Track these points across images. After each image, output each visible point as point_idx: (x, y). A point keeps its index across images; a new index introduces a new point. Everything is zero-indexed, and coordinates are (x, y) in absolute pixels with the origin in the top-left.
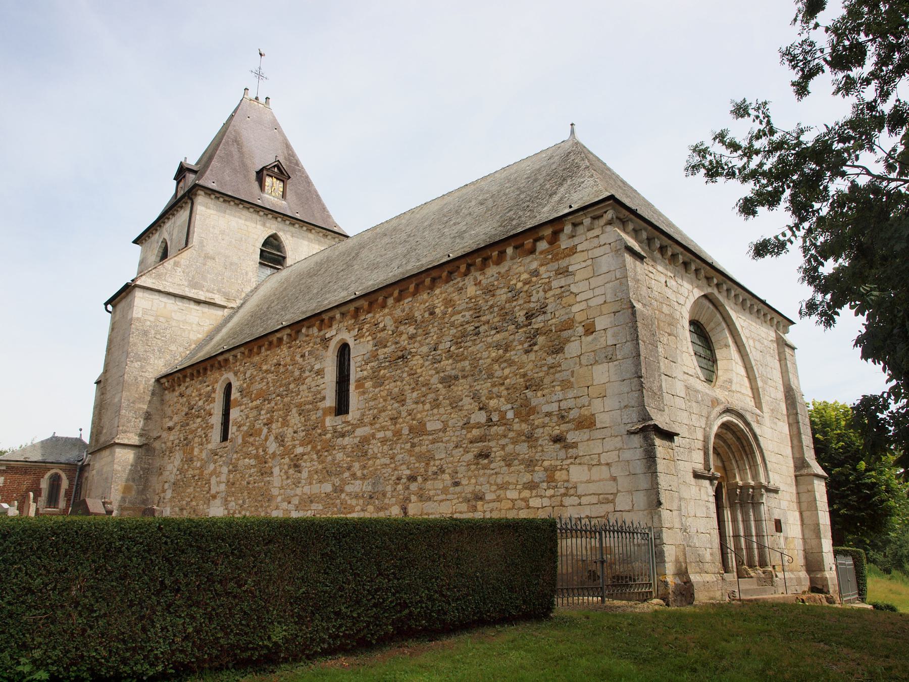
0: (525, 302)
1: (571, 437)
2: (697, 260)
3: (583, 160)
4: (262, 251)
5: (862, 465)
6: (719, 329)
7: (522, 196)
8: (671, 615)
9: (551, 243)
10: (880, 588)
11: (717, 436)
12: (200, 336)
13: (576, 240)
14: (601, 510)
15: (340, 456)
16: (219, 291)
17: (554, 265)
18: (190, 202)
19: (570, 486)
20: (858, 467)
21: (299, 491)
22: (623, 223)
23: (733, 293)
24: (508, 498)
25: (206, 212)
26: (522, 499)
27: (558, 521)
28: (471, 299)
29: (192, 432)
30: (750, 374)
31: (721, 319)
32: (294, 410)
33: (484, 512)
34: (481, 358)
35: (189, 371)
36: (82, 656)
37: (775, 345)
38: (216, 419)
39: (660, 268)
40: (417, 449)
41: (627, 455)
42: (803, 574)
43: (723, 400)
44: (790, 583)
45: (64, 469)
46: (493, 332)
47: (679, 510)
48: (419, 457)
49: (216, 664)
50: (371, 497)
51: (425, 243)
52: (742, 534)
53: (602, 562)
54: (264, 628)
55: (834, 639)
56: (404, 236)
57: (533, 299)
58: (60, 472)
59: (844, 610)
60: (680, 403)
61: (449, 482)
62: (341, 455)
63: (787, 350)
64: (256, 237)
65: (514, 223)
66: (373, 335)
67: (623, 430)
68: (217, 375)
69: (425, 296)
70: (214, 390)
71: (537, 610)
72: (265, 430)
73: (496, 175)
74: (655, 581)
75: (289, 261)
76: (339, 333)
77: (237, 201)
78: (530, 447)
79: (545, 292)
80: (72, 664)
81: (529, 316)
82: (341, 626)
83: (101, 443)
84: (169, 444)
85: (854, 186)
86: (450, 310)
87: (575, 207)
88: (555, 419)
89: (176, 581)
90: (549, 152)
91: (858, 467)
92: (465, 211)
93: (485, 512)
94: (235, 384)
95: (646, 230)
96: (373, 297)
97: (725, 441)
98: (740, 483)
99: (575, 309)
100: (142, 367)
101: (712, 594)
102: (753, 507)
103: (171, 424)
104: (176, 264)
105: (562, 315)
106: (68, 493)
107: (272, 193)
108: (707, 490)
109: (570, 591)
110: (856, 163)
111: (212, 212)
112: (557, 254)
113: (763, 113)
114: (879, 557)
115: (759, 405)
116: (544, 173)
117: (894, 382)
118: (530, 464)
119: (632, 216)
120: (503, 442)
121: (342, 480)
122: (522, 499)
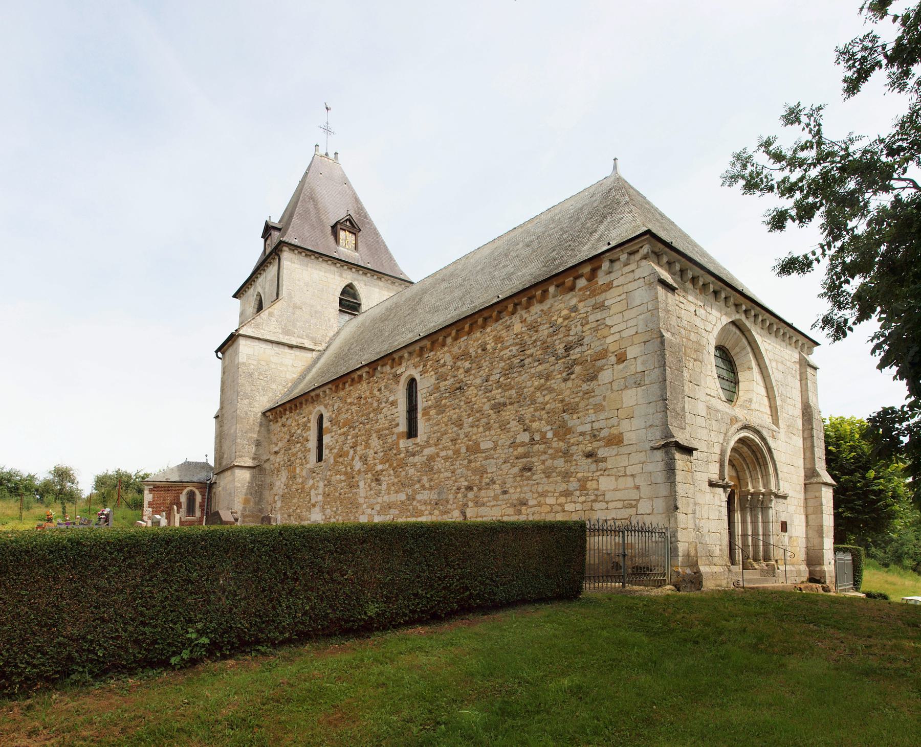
0: (565, 336)
1: (601, 453)
2: (728, 289)
3: (624, 195)
4: (341, 300)
5: (871, 474)
6: (743, 353)
7: (565, 236)
8: (680, 599)
9: (589, 280)
10: (874, 579)
11: (734, 449)
12: (295, 376)
13: (613, 276)
14: (625, 513)
15: (411, 471)
16: (307, 336)
17: (592, 301)
18: (277, 257)
19: (599, 493)
20: (867, 475)
21: (380, 500)
22: (657, 255)
23: (760, 318)
24: (547, 505)
25: (289, 261)
26: (558, 505)
27: (587, 522)
28: (517, 335)
29: (294, 455)
30: (770, 393)
31: (746, 343)
32: (374, 435)
33: (528, 515)
34: (525, 387)
35: (288, 406)
36: (231, 627)
37: (798, 366)
38: (312, 444)
39: (691, 298)
40: (473, 465)
41: (650, 467)
42: (804, 568)
43: (742, 418)
44: (790, 573)
45: (197, 488)
46: (537, 363)
47: (694, 513)
48: (475, 471)
49: (327, 632)
50: (437, 504)
51: (478, 286)
52: (750, 533)
53: (624, 556)
54: (362, 606)
55: (823, 621)
56: (460, 280)
57: (572, 333)
58: (194, 489)
59: (836, 598)
60: (700, 421)
61: (499, 491)
62: (412, 470)
63: (809, 370)
64: (335, 287)
65: (556, 262)
66: (435, 370)
67: (647, 446)
68: (311, 408)
69: (478, 334)
70: (309, 421)
71: (569, 593)
72: (352, 452)
73: (542, 216)
74: (669, 572)
75: (364, 308)
76: (408, 370)
77: (317, 255)
78: (566, 461)
79: (583, 326)
80: (224, 633)
81: (568, 349)
82: (418, 604)
83: (223, 467)
84: (276, 465)
85: (897, 201)
86: (499, 345)
87: (613, 244)
88: (588, 437)
89: (295, 573)
90: (592, 190)
91: (867, 475)
92: (513, 254)
93: (528, 515)
94: (326, 416)
95: (679, 261)
96: (435, 337)
97: (741, 455)
98: (752, 491)
99: (609, 340)
100: (250, 404)
101: (718, 582)
102: (762, 511)
103: (276, 449)
104: (271, 315)
105: (597, 346)
106: (201, 505)
107: (346, 245)
108: (721, 496)
109: (597, 578)
110: (902, 177)
111: (296, 266)
112: (595, 290)
113: (815, 121)
114: (880, 553)
115: (776, 421)
116: (586, 212)
117: (913, 398)
118: (566, 476)
119: (667, 249)
120: (543, 457)
121: (414, 491)
122: (558, 505)
